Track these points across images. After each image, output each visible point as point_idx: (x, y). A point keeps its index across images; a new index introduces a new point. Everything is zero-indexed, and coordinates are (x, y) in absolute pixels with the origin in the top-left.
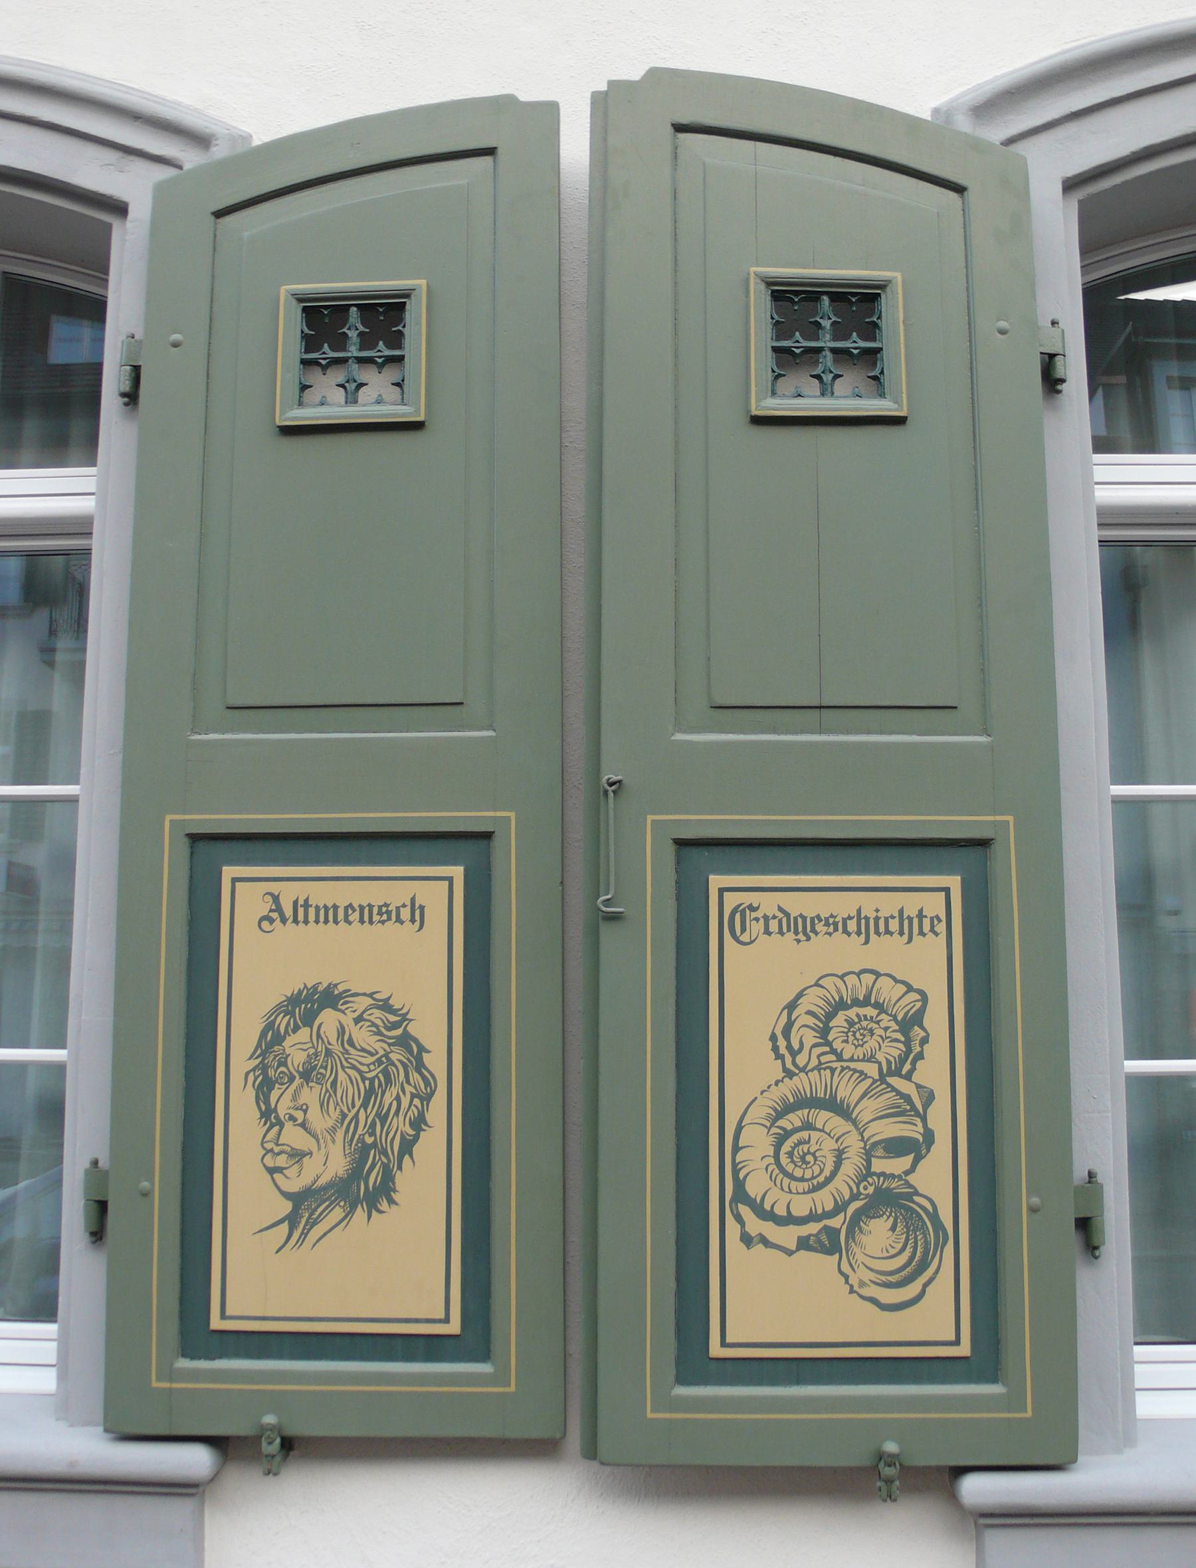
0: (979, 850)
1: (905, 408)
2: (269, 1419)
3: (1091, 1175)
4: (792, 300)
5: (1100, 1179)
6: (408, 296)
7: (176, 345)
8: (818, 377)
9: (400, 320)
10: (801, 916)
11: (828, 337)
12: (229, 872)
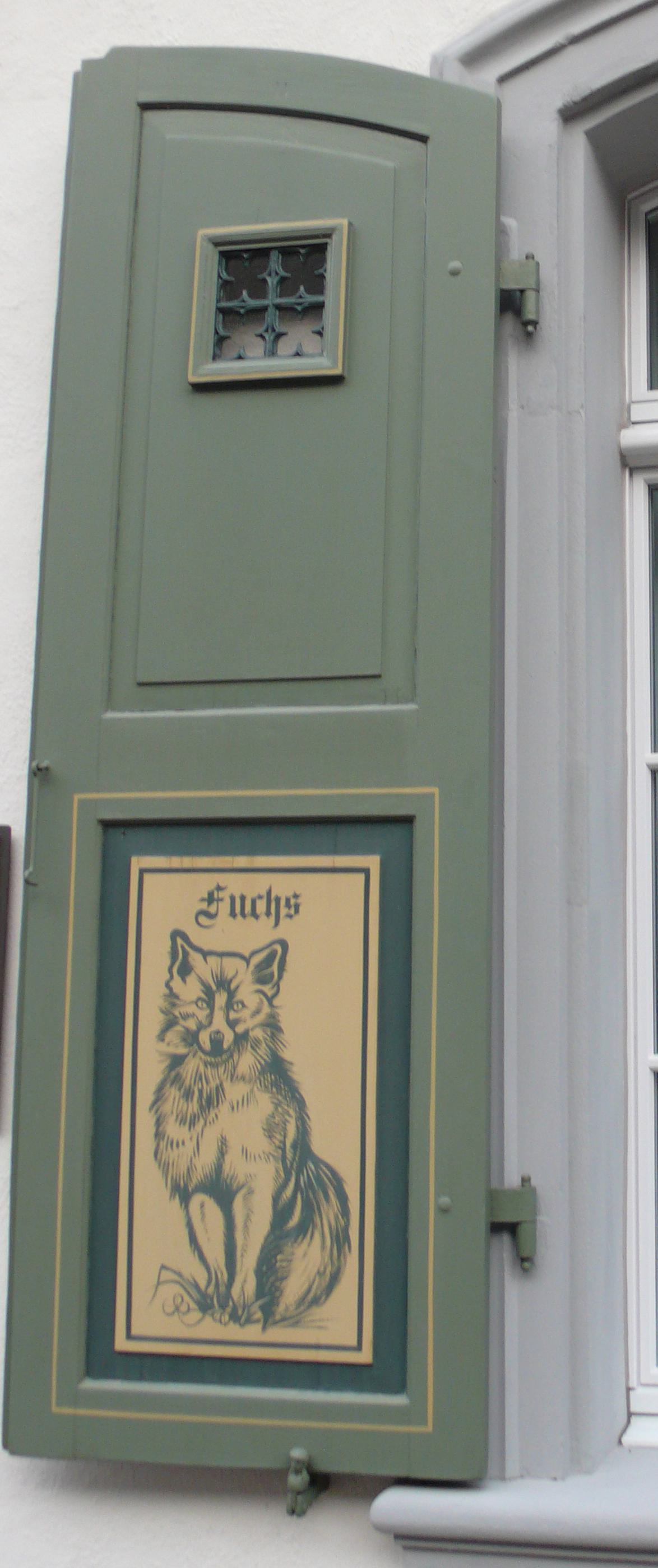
1: (340, 365)
2: (298, 1453)
3: (525, 1180)
4: (241, 262)
5: (534, 1182)
6: (329, 236)
7: (455, 273)
8: (262, 336)
9: (323, 261)
12: (137, 863)
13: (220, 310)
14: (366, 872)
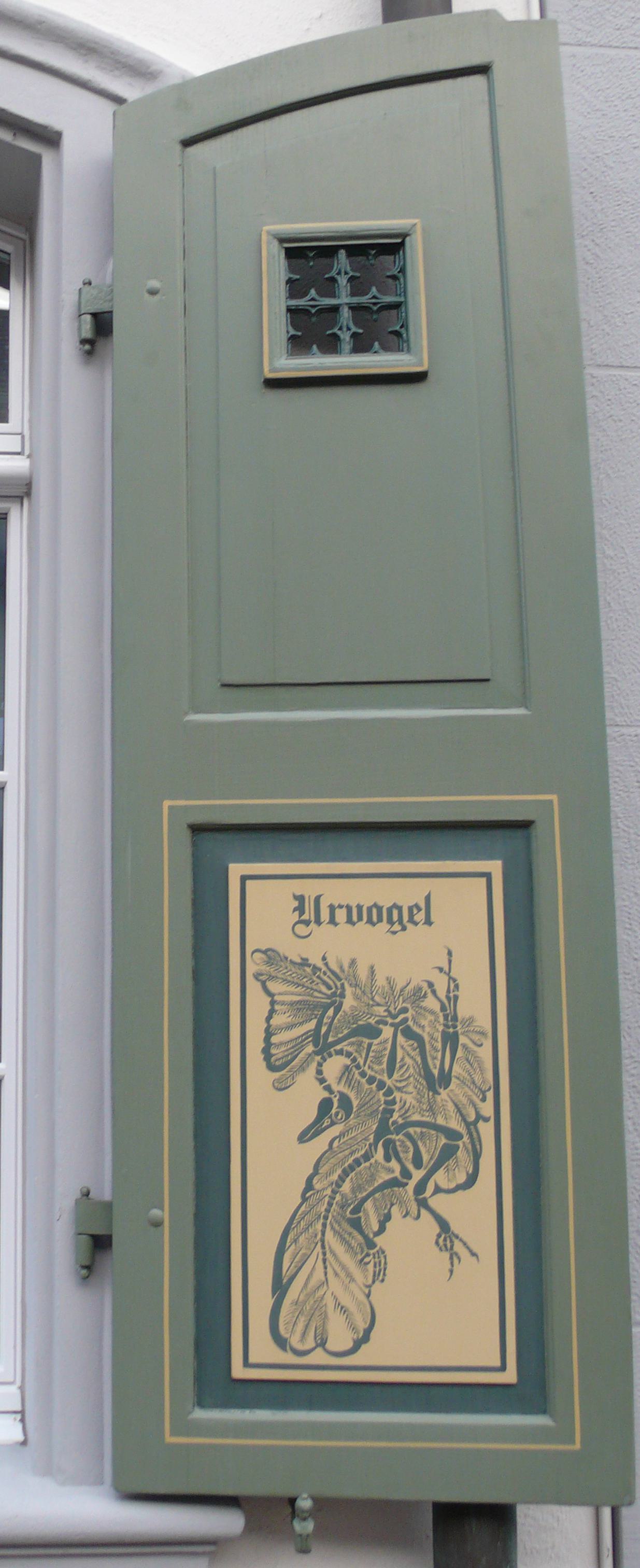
0: (519, 833)
4: (307, 258)
10: (375, 905)
11: (344, 294)
13: (289, 310)
14: (488, 876)
